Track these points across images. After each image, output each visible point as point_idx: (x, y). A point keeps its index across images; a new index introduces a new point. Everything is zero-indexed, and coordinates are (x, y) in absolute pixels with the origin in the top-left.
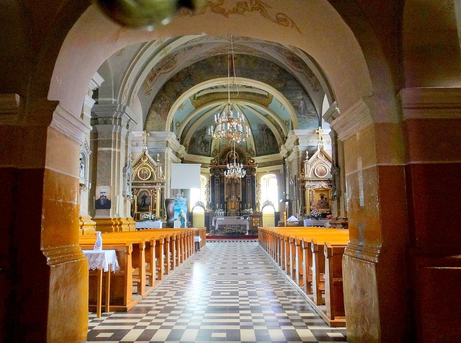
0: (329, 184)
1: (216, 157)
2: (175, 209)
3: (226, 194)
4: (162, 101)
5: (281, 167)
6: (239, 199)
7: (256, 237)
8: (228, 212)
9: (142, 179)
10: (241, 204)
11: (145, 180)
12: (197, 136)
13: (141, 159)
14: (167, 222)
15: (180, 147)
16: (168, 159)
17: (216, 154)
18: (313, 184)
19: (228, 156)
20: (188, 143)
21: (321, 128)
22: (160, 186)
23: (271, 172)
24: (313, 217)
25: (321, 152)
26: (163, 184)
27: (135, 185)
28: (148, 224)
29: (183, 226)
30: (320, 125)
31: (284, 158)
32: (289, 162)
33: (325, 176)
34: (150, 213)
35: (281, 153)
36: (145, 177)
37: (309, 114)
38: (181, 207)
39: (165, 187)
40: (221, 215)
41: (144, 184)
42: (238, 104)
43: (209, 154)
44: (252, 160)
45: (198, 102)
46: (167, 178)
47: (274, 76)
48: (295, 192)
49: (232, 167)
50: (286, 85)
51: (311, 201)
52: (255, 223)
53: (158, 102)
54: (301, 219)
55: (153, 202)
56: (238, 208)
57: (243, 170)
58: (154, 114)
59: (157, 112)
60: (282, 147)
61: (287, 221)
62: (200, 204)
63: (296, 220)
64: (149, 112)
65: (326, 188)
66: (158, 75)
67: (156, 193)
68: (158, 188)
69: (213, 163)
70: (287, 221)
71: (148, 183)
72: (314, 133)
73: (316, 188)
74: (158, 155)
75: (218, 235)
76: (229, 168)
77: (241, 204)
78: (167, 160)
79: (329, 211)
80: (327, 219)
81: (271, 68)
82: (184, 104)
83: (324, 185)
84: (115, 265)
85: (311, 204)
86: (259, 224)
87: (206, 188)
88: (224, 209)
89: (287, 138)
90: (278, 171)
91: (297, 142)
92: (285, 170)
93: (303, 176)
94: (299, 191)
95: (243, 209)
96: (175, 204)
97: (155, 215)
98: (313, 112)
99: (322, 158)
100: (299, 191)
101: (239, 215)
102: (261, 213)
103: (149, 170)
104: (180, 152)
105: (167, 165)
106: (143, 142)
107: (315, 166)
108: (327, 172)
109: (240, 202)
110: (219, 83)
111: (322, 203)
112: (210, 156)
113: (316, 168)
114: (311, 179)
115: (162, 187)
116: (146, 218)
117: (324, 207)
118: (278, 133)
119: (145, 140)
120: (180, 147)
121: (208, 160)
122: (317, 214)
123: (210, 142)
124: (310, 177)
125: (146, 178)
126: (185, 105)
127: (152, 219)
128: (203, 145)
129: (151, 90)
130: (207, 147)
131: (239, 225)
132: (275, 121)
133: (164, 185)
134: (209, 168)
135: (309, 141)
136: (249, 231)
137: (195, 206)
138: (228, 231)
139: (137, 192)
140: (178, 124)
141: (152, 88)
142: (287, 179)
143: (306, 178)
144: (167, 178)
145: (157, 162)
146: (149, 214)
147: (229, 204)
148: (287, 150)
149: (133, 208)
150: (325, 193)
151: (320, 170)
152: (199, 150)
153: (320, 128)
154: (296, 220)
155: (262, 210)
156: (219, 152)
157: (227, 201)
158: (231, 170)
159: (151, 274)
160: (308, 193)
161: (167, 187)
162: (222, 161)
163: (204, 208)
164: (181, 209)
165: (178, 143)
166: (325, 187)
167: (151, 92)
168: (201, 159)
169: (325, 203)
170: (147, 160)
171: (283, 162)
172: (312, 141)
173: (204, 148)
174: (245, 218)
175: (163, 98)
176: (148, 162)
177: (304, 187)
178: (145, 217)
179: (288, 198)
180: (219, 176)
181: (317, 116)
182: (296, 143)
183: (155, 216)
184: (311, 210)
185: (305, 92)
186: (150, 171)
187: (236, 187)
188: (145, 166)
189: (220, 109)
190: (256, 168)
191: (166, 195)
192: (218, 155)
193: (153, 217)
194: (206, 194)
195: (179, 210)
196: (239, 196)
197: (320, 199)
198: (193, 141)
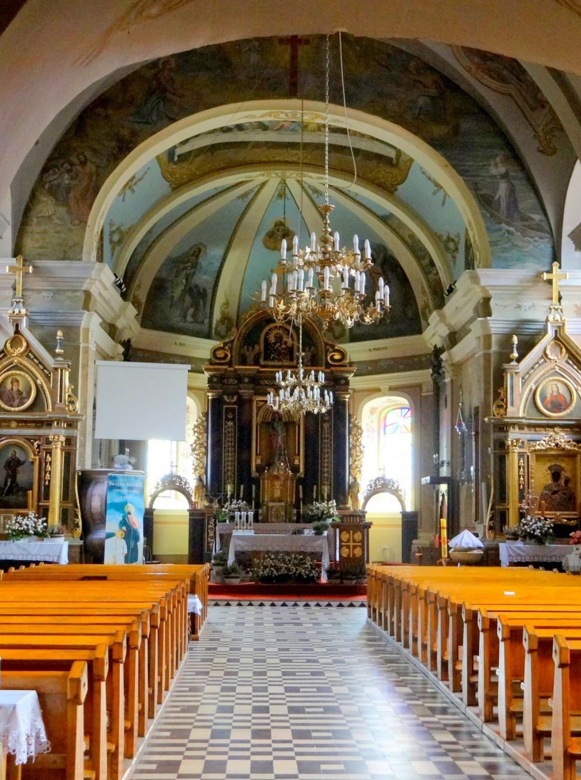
0: (575, 437)
1: (227, 340)
2: (108, 502)
3: (257, 454)
4: (72, 164)
5: (424, 376)
6: (295, 469)
7: (357, 591)
8: (260, 511)
9: (6, 407)
10: (301, 487)
11: (17, 409)
12: (174, 275)
14: (81, 543)
15: (123, 309)
16: (90, 346)
17: (229, 329)
18: (529, 437)
19: (266, 340)
20: (143, 295)
21: (560, 268)
22: (63, 431)
23: (395, 390)
24: (528, 536)
25: (556, 338)
26: (71, 424)
28: (25, 547)
29: (131, 557)
30: (556, 257)
31: (438, 352)
32: (452, 365)
33: (568, 411)
34: (32, 514)
35: (427, 333)
36: (17, 401)
38: (129, 498)
39: (77, 433)
40: (244, 519)
41: (14, 424)
42: (305, 179)
43: (205, 328)
44: (339, 351)
45: (183, 171)
46: (84, 406)
47: (421, 101)
48: (474, 454)
49: (291, 380)
50: (456, 131)
51: (521, 487)
52: (348, 547)
53: (61, 169)
54: (490, 542)
55: (40, 478)
56: (291, 499)
57: (326, 392)
58: (46, 206)
59: (56, 199)
60: (434, 317)
61: (448, 546)
62: (175, 483)
63: (477, 542)
64: (33, 196)
65: (568, 447)
67: (49, 452)
68: (58, 435)
69: (219, 359)
70: (450, 546)
71: (25, 422)
72: (538, 282)
73: (538, 447)
74: (60, 333)
75: (236, 582)
76: (283, 384)
77: (301, 487)
78: (86, 350)
79: (574, 519)
80: (571, 541)
81: (411, 76)
82: (138, 177)
83: (563, 441)
84: (38, 737)
85: (522, 497)
86: (361, 550)
87: (196, 434)
88: (249, 502)
89: (451, 290)
90: (418, 389)
91: (485, 308)
92: (438, 389)
93: (502, 411)
94: (485, 454)
95: (308, 499)
96: (111, 488)
97: (46, 521)
98: (537, 217)
99: (559, 359)
100: (485, 454)
101: (295, 518)
102: (362, 515)
103: (30, 379)
104: (120, 324)
105: (85, 366)
106: (11, 292)
107: (537, 381)
108: (571, 400)
109: (300, 481)
110: (254, 117)
111: (555, 493)
112: (208, 336)
113: (541, 386)
114: (524, 421)
115: (71, 432)
116: (20, 529)
117: (561, 506)
118: (420, 275)
119: (19, 287)
120: (123, 309)
121: (203, 348)
122: (541, 528)
123: (210, 292)
126: (140, 180)
127: (36, 533)
128: (188, 300)
130: (202, 308)
131: (301, 553)
132: (412, 236)
133: (76, 428)
134: (207, 375)
135: (520, 303)
136: (331, 573)
137: (162, 490)
138: (268, 570)
140: (116, 238)
142: (445, 414)
143: (511, 418)
144: (84, 406)
145: (54, 355)
146: (27, 515)
147: (266, 484)
148: (449, 326)
150: (563, 465)
151: (552, 394)
152: (175, 318)
153: (556, 265)
154: (477, 542)
156: (237, 326)
157: (258, 474)
158: (289, 389)
159: (114, 747)
160: (514, 462)
161: (84, 435)
162: (247, 354)
163: (188, 496)
164: (126, 503)
165: (114, 296)
166: (567, 446)
168: (181, 344)
169: (564, 494)
170: (23, 349)
171: (433, 361)
172: (530, 304)
173: (191, 311)
174: (319, 531)
175: (78, 156)
176: (28, 356)
177: (502, 447)
178: (17, 527)
179: (444, 472)
180: (235, 398)
181: (548, 229)
182: (480, 310)
183: (45, 524)
184: (522, 515)
185: (515, 156)
187: (287, 431)
188: (16, 367)
189: (245, 195)
190: (351, 377)
191: (80, 458)
192: (234, 335)
193: (42, 526)
195: (120, 507)
196: (296, 462)
197: (550, 482)
198: (159, 287)
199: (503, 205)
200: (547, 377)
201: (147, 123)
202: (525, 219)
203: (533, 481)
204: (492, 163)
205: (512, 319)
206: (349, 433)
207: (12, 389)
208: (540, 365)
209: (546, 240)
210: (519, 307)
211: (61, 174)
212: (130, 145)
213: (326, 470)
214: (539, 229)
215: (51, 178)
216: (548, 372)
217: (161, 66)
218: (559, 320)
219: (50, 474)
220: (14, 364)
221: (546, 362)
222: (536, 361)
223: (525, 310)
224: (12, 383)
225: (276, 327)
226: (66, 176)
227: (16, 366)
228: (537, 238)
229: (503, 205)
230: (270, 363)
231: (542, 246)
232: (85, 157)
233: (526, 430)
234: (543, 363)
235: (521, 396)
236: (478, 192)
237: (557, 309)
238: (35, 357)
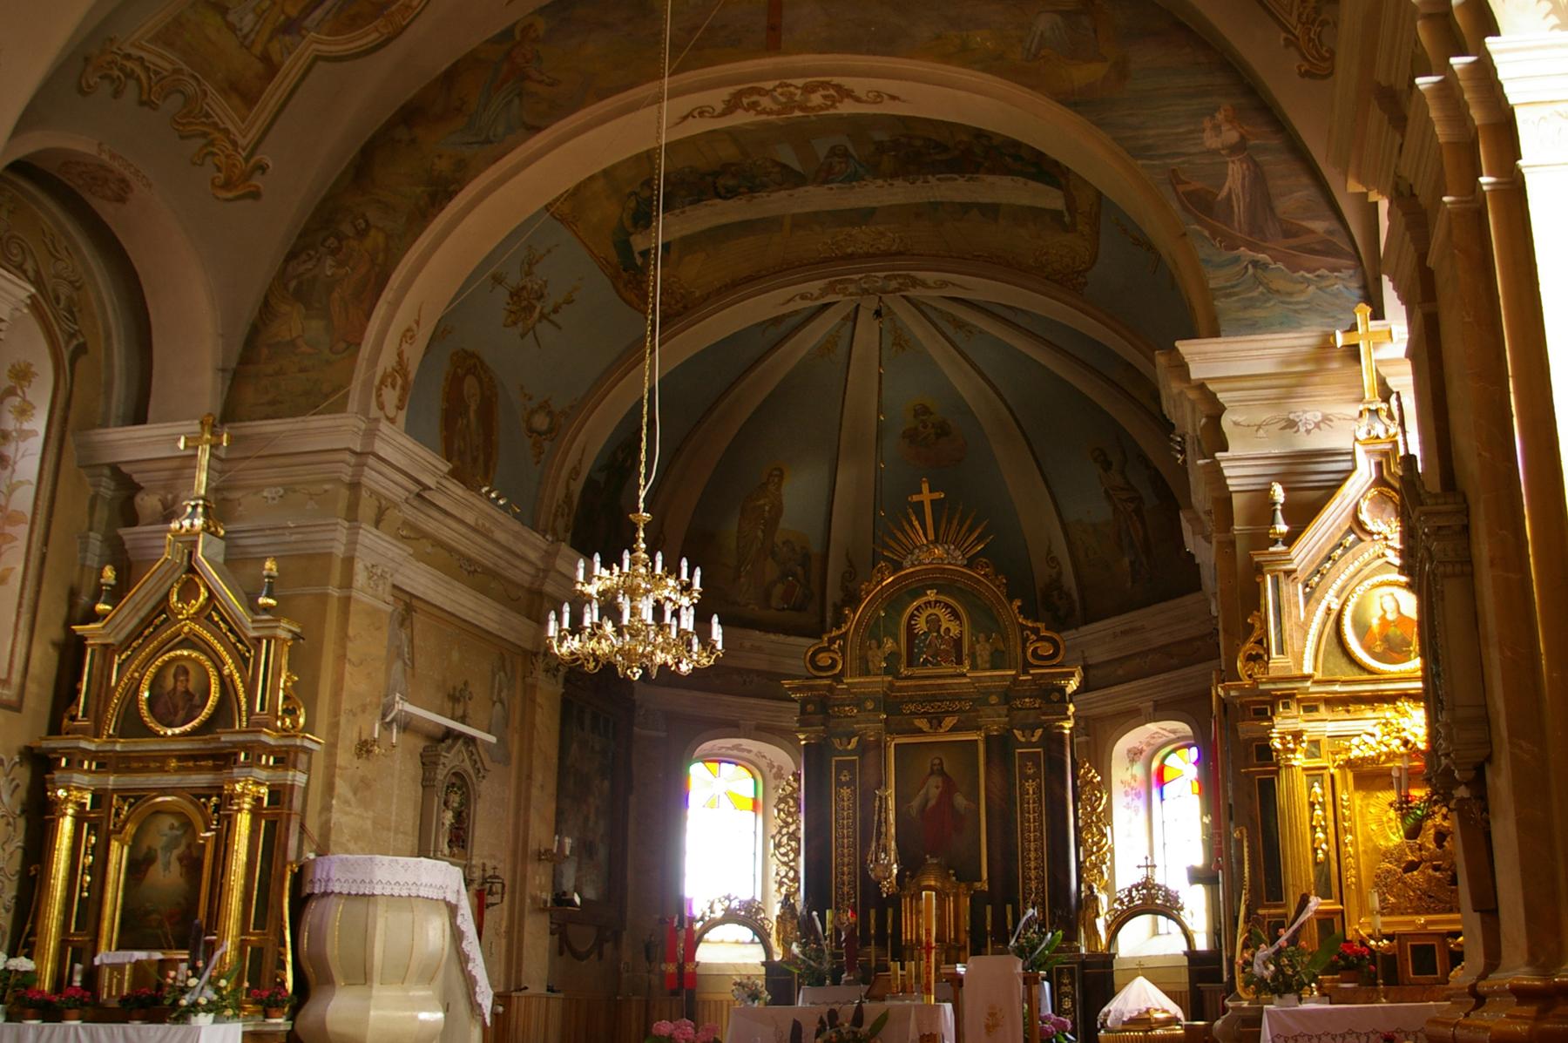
13: (166, 597)
18: (1331, 728)
19: (910, 628)
27: (117, 771)
36: (181, 714)
37: (1292, 242)
64: (266, 310)
66: (291, 68)
107: (1343, 589)
111: (1411, 867)
124: (1307, 669)
129: (263, 168)
140: (541, 422)
141: (264, 156)
151: (1383, 618)
155: (1113, 937)
163: (762, 935)
167: (257, 181)
181: (1349, 249)
186: (212, 673)
188: (187, 643)
194: (783, 850)
199: (1239, 208)
200: (1366, 578)
201: (488, 141)
202: (1290, 232)
203: (1349, 837)
204: (1207, 123)
205: (1276, 451)
206: (1076, 799)
208: (1346, 549)
209: (1346, 274)
210: (1292, 424)
211: (319, 259)
212: (452, 188)
213: (1033, 874)
214: (1328, 249)
215: (302, 269)
216: (1367, 564)
217: (518, 36)
218: (1383, 435)
220: (183, 636)
221: (1361, 540)
222: (1336, 540)
223: (1308, 431)
224: (175, 676)
225: (929, 602)
226: (329, 261)
228: (1323, 272)
229: (1239, 208)
230: (918, 672)
231: (1339, 286)
232: (367, 221)
233: (1323, 711)
234: (1353, 545)
235: (1304, 628)
236: (1181, 188)
237: (1376, 412)
238: (223, 619)
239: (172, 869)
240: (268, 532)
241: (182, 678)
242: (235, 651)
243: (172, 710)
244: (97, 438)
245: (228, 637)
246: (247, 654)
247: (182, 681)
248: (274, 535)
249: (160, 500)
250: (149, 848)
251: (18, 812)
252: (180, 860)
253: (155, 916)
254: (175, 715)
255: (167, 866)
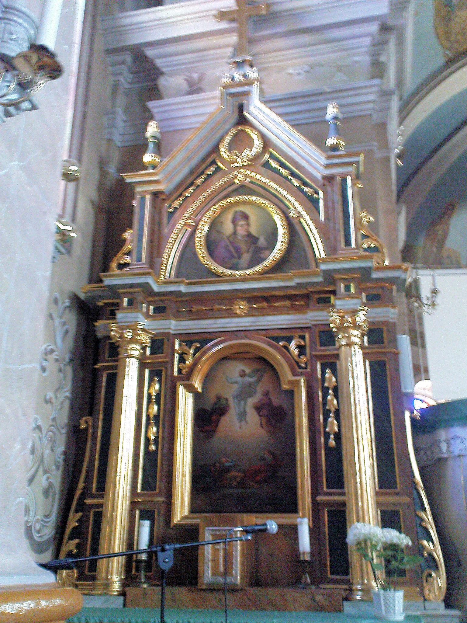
13: (216, 149)
27: (178, 315)
36: (246, 257)
41: (241, 307)
125: (249, 267)
139: (190, 361)
149: (160, 484)
188: (242, 189)
207: (235, 233)
219: (336, 396)
224: (234, 221)
227: (242, 186)
239: (248, 418)
240: (301, 100)
241: (242, 223)
242: (301, 194)
243: (235, 254)
244: (126, 21)
245: (290, 181)
246: (315, 196)
247: (242, 226)
248: (307, 102)
249: (186, 80)
250: (219, 398)
251: (67, 360)
252: (258, 408)
253: (234, 473)
254: (239, 258)
255: (242, 415)
